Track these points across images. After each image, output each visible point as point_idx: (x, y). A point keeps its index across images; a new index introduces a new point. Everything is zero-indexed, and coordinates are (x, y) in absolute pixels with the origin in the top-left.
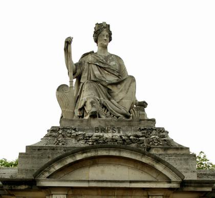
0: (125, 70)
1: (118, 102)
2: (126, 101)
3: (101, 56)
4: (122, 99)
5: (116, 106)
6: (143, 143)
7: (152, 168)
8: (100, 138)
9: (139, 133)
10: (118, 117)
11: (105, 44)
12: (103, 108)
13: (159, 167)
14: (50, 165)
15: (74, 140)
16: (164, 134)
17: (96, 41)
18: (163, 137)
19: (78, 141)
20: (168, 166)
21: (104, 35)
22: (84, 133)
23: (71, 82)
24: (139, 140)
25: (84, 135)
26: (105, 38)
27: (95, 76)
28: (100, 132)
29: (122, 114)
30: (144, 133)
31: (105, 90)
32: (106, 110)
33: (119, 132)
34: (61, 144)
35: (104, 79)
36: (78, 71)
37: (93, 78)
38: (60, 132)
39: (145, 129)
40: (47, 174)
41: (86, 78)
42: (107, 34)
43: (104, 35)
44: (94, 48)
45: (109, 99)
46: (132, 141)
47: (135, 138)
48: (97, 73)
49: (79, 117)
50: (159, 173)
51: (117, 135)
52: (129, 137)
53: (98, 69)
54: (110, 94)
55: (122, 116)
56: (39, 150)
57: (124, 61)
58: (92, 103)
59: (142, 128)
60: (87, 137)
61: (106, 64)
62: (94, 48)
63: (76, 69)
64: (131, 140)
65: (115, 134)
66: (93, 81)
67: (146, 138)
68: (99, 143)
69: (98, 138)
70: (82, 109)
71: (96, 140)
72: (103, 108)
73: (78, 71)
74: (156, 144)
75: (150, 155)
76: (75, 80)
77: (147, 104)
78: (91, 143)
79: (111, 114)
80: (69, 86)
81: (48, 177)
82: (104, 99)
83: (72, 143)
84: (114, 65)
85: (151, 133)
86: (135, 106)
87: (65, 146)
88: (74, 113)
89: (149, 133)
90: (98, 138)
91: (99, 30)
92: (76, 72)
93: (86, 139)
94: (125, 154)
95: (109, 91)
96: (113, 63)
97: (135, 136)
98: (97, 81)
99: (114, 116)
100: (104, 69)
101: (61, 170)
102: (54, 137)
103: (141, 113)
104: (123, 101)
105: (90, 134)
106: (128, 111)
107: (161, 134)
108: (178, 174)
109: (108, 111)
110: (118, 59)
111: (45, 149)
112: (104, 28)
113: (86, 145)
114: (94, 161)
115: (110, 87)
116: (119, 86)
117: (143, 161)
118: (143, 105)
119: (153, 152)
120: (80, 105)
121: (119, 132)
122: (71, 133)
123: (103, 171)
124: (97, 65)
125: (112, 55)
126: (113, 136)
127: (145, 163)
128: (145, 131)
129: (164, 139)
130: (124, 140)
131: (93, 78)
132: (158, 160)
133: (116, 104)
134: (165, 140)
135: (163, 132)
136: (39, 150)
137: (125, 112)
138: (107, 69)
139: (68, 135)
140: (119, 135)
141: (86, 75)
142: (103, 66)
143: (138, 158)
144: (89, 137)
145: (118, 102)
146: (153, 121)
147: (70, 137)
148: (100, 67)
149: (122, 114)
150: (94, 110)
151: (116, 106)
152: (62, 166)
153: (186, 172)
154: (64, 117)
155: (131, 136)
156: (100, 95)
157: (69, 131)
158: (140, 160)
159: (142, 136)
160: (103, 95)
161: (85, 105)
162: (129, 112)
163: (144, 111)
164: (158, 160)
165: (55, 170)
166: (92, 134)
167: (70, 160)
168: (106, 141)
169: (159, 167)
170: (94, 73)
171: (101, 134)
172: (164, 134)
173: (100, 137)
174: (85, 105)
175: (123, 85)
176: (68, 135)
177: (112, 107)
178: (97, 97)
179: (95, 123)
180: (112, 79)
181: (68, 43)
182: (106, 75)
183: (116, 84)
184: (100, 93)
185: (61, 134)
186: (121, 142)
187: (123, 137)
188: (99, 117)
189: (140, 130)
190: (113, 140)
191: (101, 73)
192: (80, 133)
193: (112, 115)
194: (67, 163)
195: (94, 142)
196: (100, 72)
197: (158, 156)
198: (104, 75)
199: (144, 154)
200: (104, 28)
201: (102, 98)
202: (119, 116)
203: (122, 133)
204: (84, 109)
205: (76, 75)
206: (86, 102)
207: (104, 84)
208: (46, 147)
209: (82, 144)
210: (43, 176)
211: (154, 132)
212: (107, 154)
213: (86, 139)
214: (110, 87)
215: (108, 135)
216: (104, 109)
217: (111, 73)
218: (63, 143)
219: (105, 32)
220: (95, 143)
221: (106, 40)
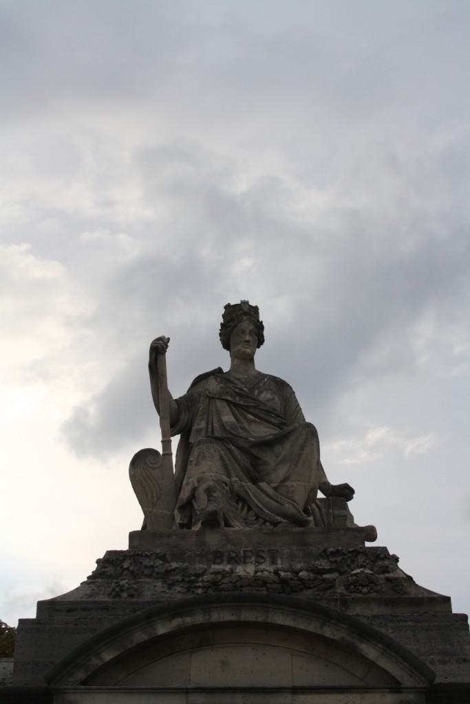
0: (298, 410)
1: (275, 489)
2: (295, 484)
3: (238, 379)
4: (283, 481)
5: (268, 495)
6: (332, 587)
7: (352, 653)
8: (224, 577)
9: (324, 564)
10: (275, 524)
11: (248, 351)
12: (237, 503)
13: (370, 651)
14: (89, 649)
15: (159, 584)
16: (386, 562)
17: (226, 345)
18: (383, 572)
19: (170, 586)
20: (390, 648)
21: (244, 332)
22: (186, 564)
23: (166, 444)
24: (324, 580)
25: (184, 570)
26: (247, 338)
27: (223, 426)
28: (225, 562)
29: (284, 516)
30: (336, 562)
31: (245, 461)
32: (246, 509)
33: (273, 562)
34: (125, 595)
35: (243, 434)
36: (184, 418)
37: (210, 434)
38: (126, 565)
39: (338, 552)
40: (81, 675)
41: (203, 433)
42: (252, 327)
43: (244, 332)
44: (223, 360)
45: (255, 481)
46: (304, 584)
47: (312, 575)
48: (228, 418)
49: (182, 526)
50: (371, 665)
51: (267, 568)
52: (297, 573)
53: (231, 410)
54: (255, 473)
55: (285, 521)
56: (70, 610)
57: (151, 342)
58: (209, 491)
59: (331, 549)
60: (191, 575)
61: (250, 398)
62: (223, 360)
63: (179, 413)
64: (301, 580)
65: (262, 567)
66: (217, 438)
67: (341, 574)
68: (222, 590)
69: (220, 577)
70: (188, 506)
71: (215, 584)
72: (237, 503)
73: (184, 418)
74: (365, 590)
75: (343, 619)
76: (175, 441)
77: (352, 491)
78: (200, 591)
79: (258, 517)
80: (161, 452)
81: (84, 683)
82: (241, 480)
83: (153, 590)
84: (269, 400)
85: (353, 561)
86: (320, 495)
87: (135, 600)
88: (173, 518)
89: (349, 562)
90: (220, 577)
91: (232, 320)
92: (178, 421)
93: (190, 581)
94: (280, 619)
95: (255, 460)
96: (265, 396)
97: (312, 571)
98: (227, 439)
99: (265, 521)
100: (246, 409)
101: (116, 662)
102: (111, 577)
103: (337, 512)
104: (288, 483)
105: (200, 567)
106: (301, 508)
107: (380, 563)
108: (416, 666)
109: (250, 509)
110: (281, 386)
111: (84, 609)
112: (245, 313)
113: (190, 596)
114: (240, 632)
115: (255, 451)
116: (278, 448)
117: (327, 635)
118: (346, 492)
119: (356, 610)
120: (185, 494)
121: (273, 562)
122: (152, 567)
123: (224, 664)
124: (227, 401)
125: (264, 376)
126: (256, 572)
127: (332, 640)
128: (339, 559)
129: (387, 575)
130: (284, 582)
131: (218, 434)
132: (366, 633)
133: (270, 491)
134: (388, 580)
135: (383, 559)
136: (70, 610)
137: (295, 511)
138: (252, 410)
139: (147, 572)
140: (271, 569)
141: (203, 424)
142: (241, 403)
143: (313, 627)
144: (197, 575)
145: (275, 489)
146: (370, 533)
147: (150, 576)
148: (236, 405)
149: (284, 516)
150: (211, 507)
151: (268, 495)
152: (117, 653)
153: (445, 663)
154: (149, 528)
155: (300, 571)
156: (232, 471)
157: (147, 562)
158: (319, 632)
159: (330, 571)
160: (239, 470)
161: (193, 496)
162: (306, 510)
163: (346, 508)
164: (366, 633)
165: (100, 663)
166: (205, 567)
167: (140, 637)
168: (239, 584)
169: (370, 651)
170: (220, 420)
171: (228, 568)
172: (386, 562)
173: (223, 574)
174: (193, 496)
175: (287, 445)
176: (147, 572)
177: (259, 500)
178: (225, 478)
179: (213, 540)
180: (262, 431)
181: (158, 350)
182: (250, 422)
183: (267, 444)
184: (230, 467)
185: (127, 569)
186: (275, 586)
187: (282, 574)
188: (227, 525)
189: (325, 554)
190: (258, 582)
191: (237, 420)
192: (174, 565)
193: (261, 521)
194: (133, 645)
195: (209, 587)
196: (234, 414)
197: (365, 621)
198: (246, 425)
199: (325, 616)
200: (245, 313)
201: (234, 479)
202: (280, 522)
203: (279, 564)
204: (192, 506)
205: (178, 427)
206: (195, 489)
207: (241, 443)
208: (87, 603)
209: (178, 594)
210: (71, 680)
211: (361, 559)
212: (260, 619)
213: (190, 582)
214: (255, 451)
215: (246, 570)
216: (240, 505)
217: (261, 419)
218: (131, 591)
219: (246, 325)
220: (210, 591)
221: (248, 341)
